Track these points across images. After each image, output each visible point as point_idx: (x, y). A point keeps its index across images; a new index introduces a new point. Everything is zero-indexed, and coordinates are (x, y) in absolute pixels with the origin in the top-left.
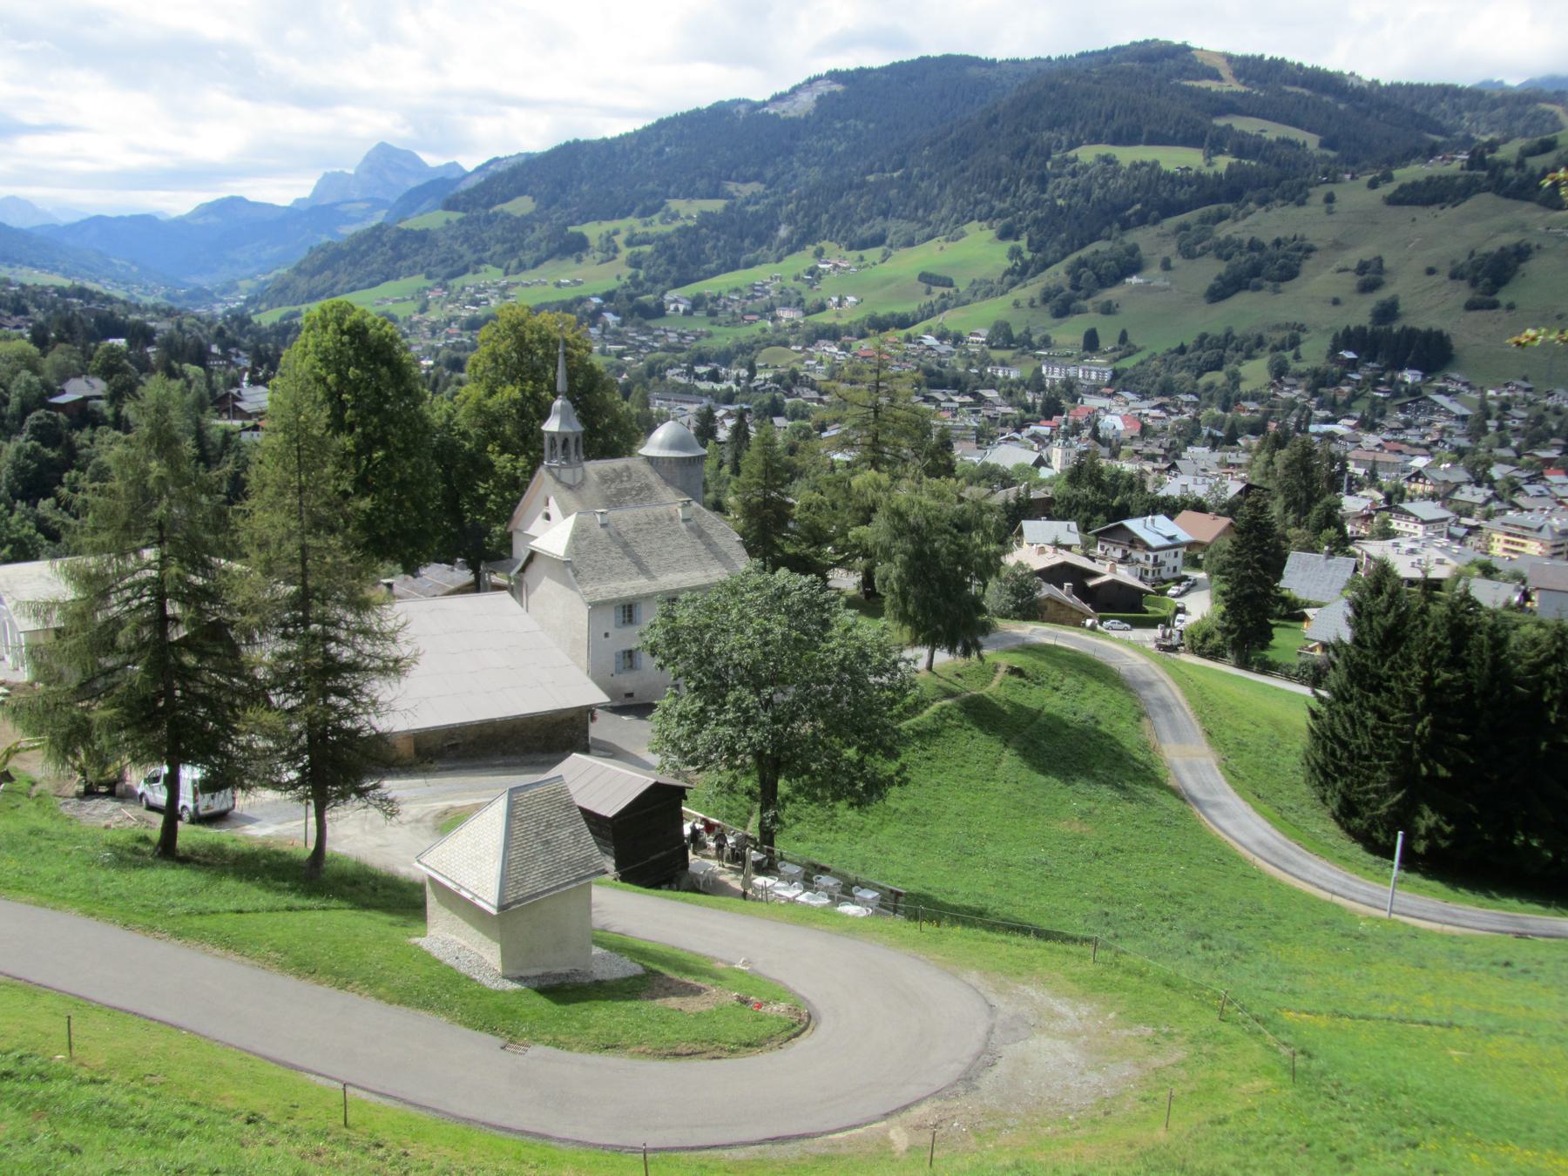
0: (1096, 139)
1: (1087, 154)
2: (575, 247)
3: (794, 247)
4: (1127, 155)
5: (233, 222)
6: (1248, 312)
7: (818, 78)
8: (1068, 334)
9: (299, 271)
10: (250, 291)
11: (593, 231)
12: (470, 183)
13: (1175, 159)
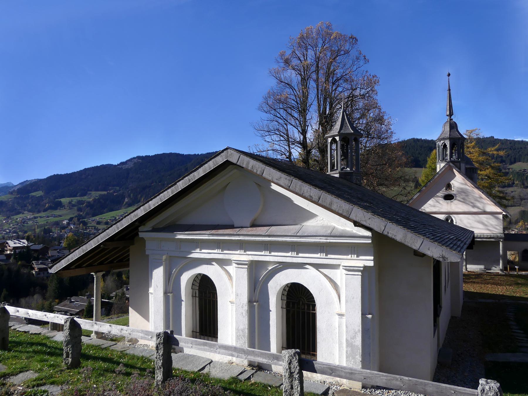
2: (58, 205)
7: (134, 158)
11: (65, 201)
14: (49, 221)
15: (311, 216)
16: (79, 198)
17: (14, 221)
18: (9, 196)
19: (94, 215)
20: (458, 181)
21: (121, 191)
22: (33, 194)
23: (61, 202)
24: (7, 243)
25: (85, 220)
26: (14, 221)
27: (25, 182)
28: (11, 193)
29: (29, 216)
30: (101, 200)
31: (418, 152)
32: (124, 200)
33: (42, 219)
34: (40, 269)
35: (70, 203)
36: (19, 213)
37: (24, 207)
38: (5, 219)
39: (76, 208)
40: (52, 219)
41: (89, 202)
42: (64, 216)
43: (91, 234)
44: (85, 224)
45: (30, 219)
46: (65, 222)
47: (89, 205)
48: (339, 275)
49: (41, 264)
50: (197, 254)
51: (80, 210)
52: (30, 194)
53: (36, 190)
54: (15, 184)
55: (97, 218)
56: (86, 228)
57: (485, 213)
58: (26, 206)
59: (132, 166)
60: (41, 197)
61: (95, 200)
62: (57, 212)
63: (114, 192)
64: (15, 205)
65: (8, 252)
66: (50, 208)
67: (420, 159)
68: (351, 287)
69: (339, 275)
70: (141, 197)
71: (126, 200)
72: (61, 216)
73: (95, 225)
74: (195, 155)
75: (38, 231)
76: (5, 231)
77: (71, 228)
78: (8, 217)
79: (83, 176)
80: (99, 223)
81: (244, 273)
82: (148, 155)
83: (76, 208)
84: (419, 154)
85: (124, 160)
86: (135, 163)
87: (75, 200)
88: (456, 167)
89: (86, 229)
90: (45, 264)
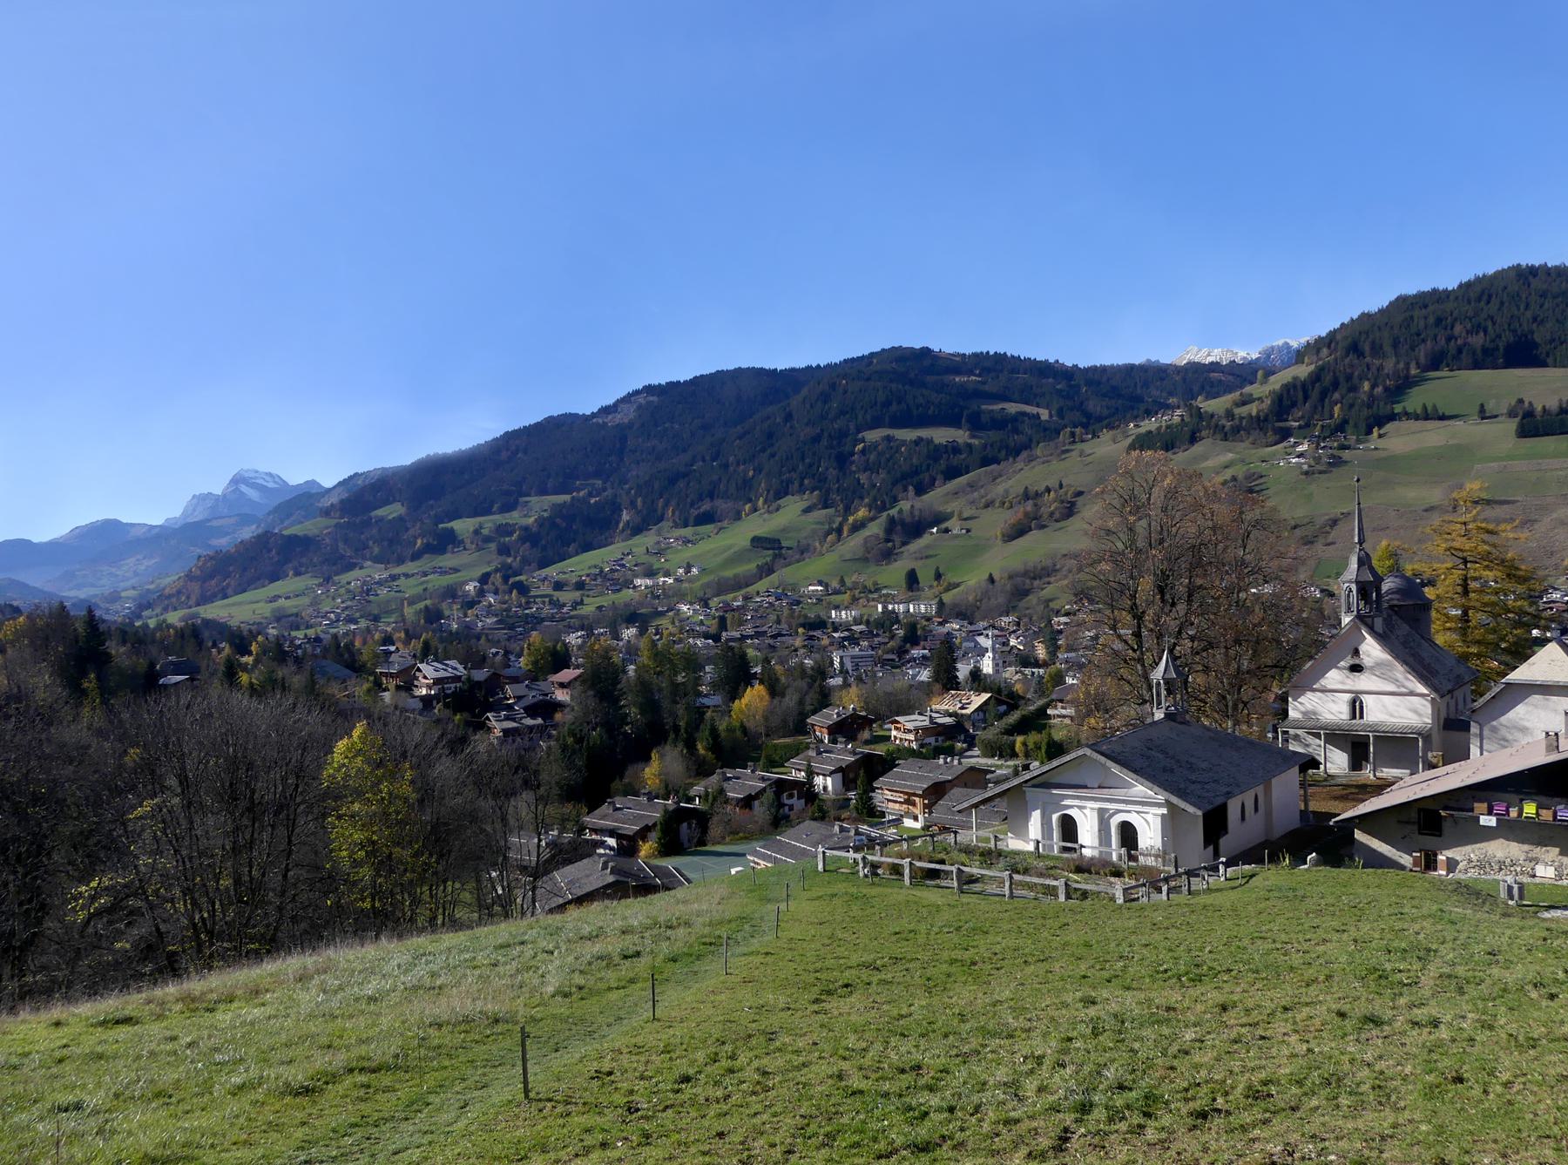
0: (876, 424)
1: (873, 436)
2: (445, 542)
3: (637, 530)
4: (907, 435)
5: (106, 539)
6: (1035, 548)
7: (637, 393)
8: (893, 574)
9: (190, 577)
10: (134, 599)
11: (463, 526)
12: (334, 499)
13: (941, 435)
14: (430, 586)
15: (1131, 786)
16: (499, 519)
17: (342, 591)
18: (322, 522)
19: (543, 564)
20: (1371, 650)
21: (609, 492)
22: (380, 512)
23: (452, 531)
24: (419, 670)
25: (522, 578)
26: (342, 591)
27: (351, 478)
28: (326, 513)
29: (378, 573)
30: (558, 520)
31: (1529, 314)
32: (620, 516)
33: (412, 581)
34: (506, 732)
35: (476, 532)
36: (351, 567)
37: (361, 549)
38: (320, 585)
39: (493, 546)
40: (438, 582)
41: (526, 529)
42: (467, 569)
43: (543, 620)
44: (523, 589)
45: (380, 583)
46: (470, 587)
47: (529, 536)
48: (1149, 817)
49: (507, 718)
50: (1067, 802)
51: (504, 550)
52: (373, 514)
53: (386, 502)
54: (328, 483)
55: (552, 571)
56: (528, 603)
57: (1412, 694)
58: (366, 547)
59: (632, 416)
60: (400, 519)
61: (541, 522)
62: (447, 560)
63: (590, 495)
64: (341, 545)
65: (424, 692)
66: (430, 549)
67: (1537, 338)
68: (1157, 824)
69: (1149, 817)
70: (666, 505)
71: (625, 516)
72: (456, 570)
73: (550, 591)
74: (809, 368)
75: (409, 611)
76: (325, 617)
77: (490, 605)
78: (328, 580)
79: (504, 455)
80: (559, 586)
81: (1095, 814)
82: (674, 380)
83: (493, 546)
84: (1535, 319)
85: (610, 401)
86: (640, 407)
87: (489, 522)
88: (1366, 625)
89: (528, 605)
90: (514, 720)
